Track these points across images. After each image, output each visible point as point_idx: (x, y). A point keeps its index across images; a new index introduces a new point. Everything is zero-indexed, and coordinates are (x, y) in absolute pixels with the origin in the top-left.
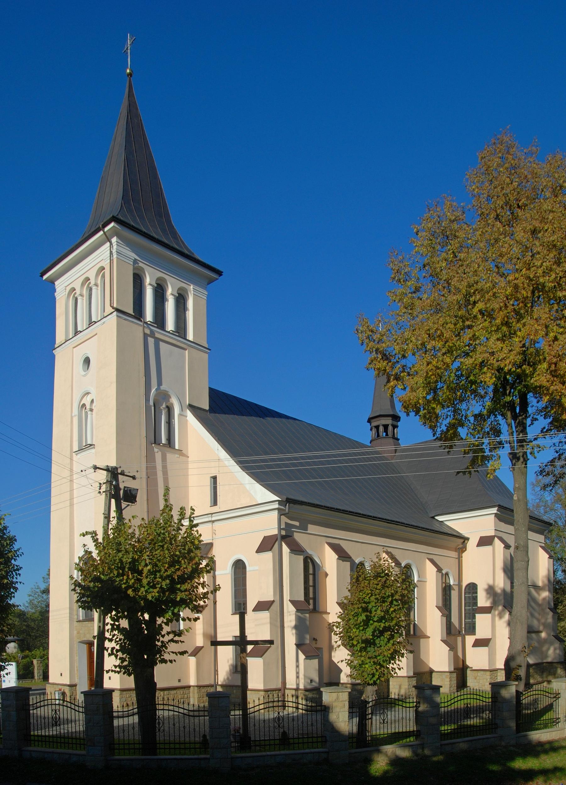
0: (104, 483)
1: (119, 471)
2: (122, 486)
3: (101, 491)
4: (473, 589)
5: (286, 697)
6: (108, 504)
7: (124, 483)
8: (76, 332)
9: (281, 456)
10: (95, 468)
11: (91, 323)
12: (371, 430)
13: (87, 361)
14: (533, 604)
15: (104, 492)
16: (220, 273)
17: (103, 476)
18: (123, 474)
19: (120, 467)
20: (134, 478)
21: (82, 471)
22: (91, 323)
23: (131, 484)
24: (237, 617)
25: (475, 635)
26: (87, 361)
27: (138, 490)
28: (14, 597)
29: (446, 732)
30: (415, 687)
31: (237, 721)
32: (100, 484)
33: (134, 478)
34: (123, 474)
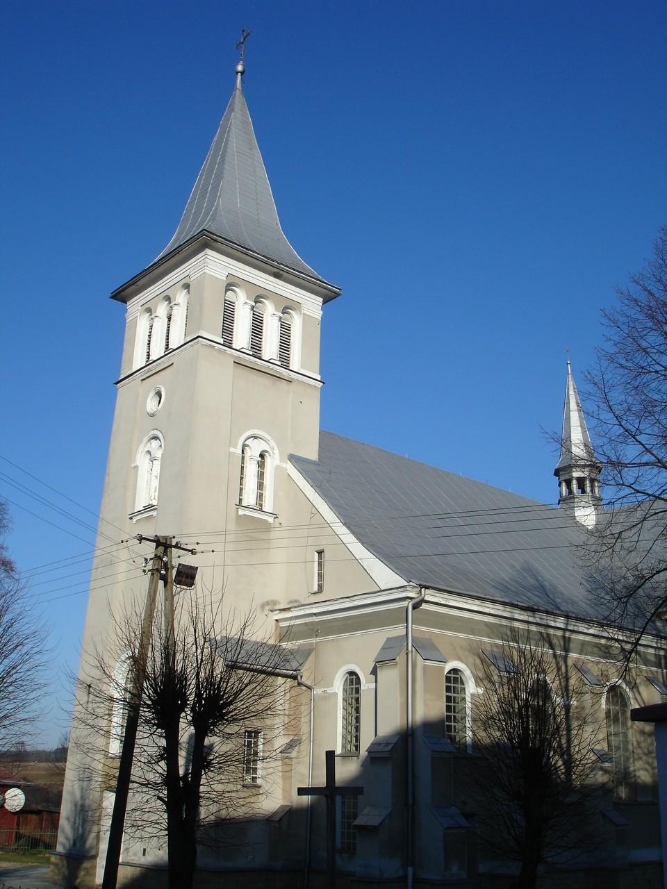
0: (151, 559)
2: (175, 562)
4: (345, 802)
7: (178, 559)
9: (214, 274)
10: (141, 539)
12: (560, 485)
14: (296, 604)
15: (149, 571)
17: (149, 549)
19: (174, 537)
20: (193, 552)
21: (122, 542)
22: (254, 314)
23: (188, 560)
27: (197, 568)
30: (290, 809)
32: (146, 559)
33: (193, 552)
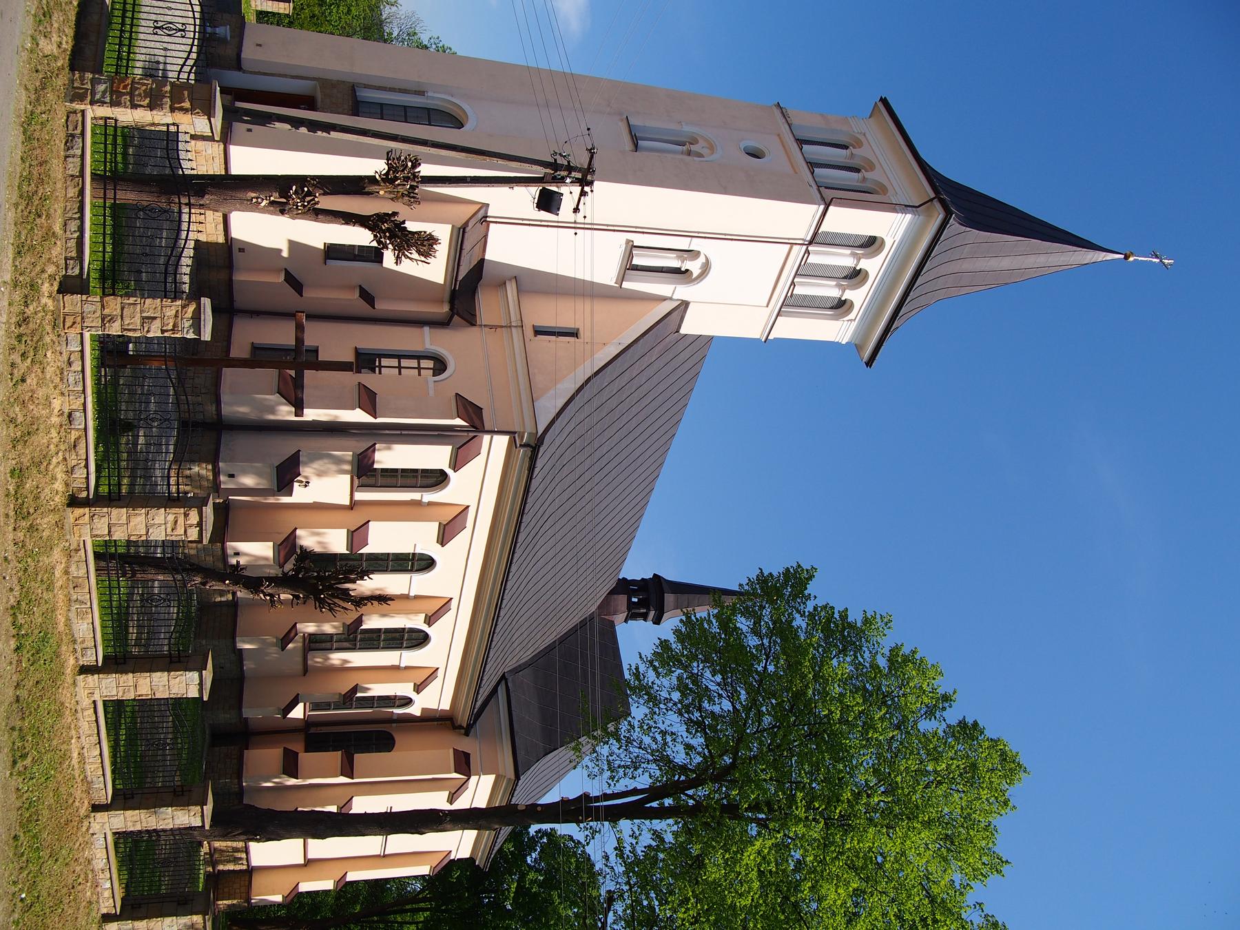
1: (587, 189)
2: (564, 190)
3: (558, 157)
5: (198, 211)
6: (500, 162)
8: (801, 142)
11: (812, 165)
13: (755, 154)
16: (869, 363)
18: (583, 193)
20: (576, 210)
22: (812, 165)
24: (349, 357)
25: (306, 751)
26: (755, 154)
28: (16, 205)
29: (198, 22)
31: (158, 648)
33: (576, 210)
34: (583, 193)
